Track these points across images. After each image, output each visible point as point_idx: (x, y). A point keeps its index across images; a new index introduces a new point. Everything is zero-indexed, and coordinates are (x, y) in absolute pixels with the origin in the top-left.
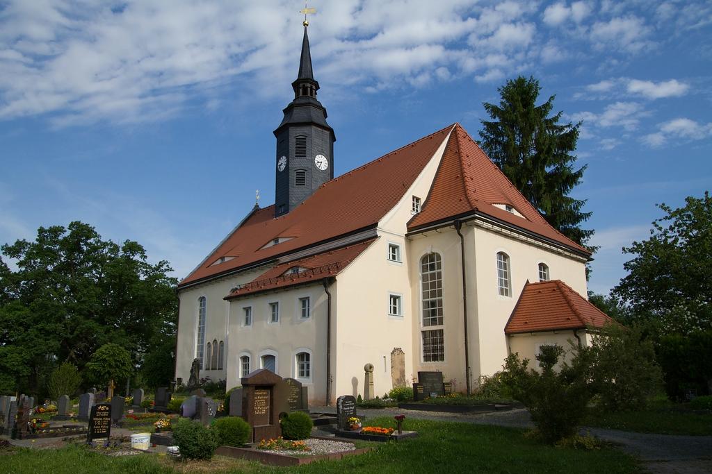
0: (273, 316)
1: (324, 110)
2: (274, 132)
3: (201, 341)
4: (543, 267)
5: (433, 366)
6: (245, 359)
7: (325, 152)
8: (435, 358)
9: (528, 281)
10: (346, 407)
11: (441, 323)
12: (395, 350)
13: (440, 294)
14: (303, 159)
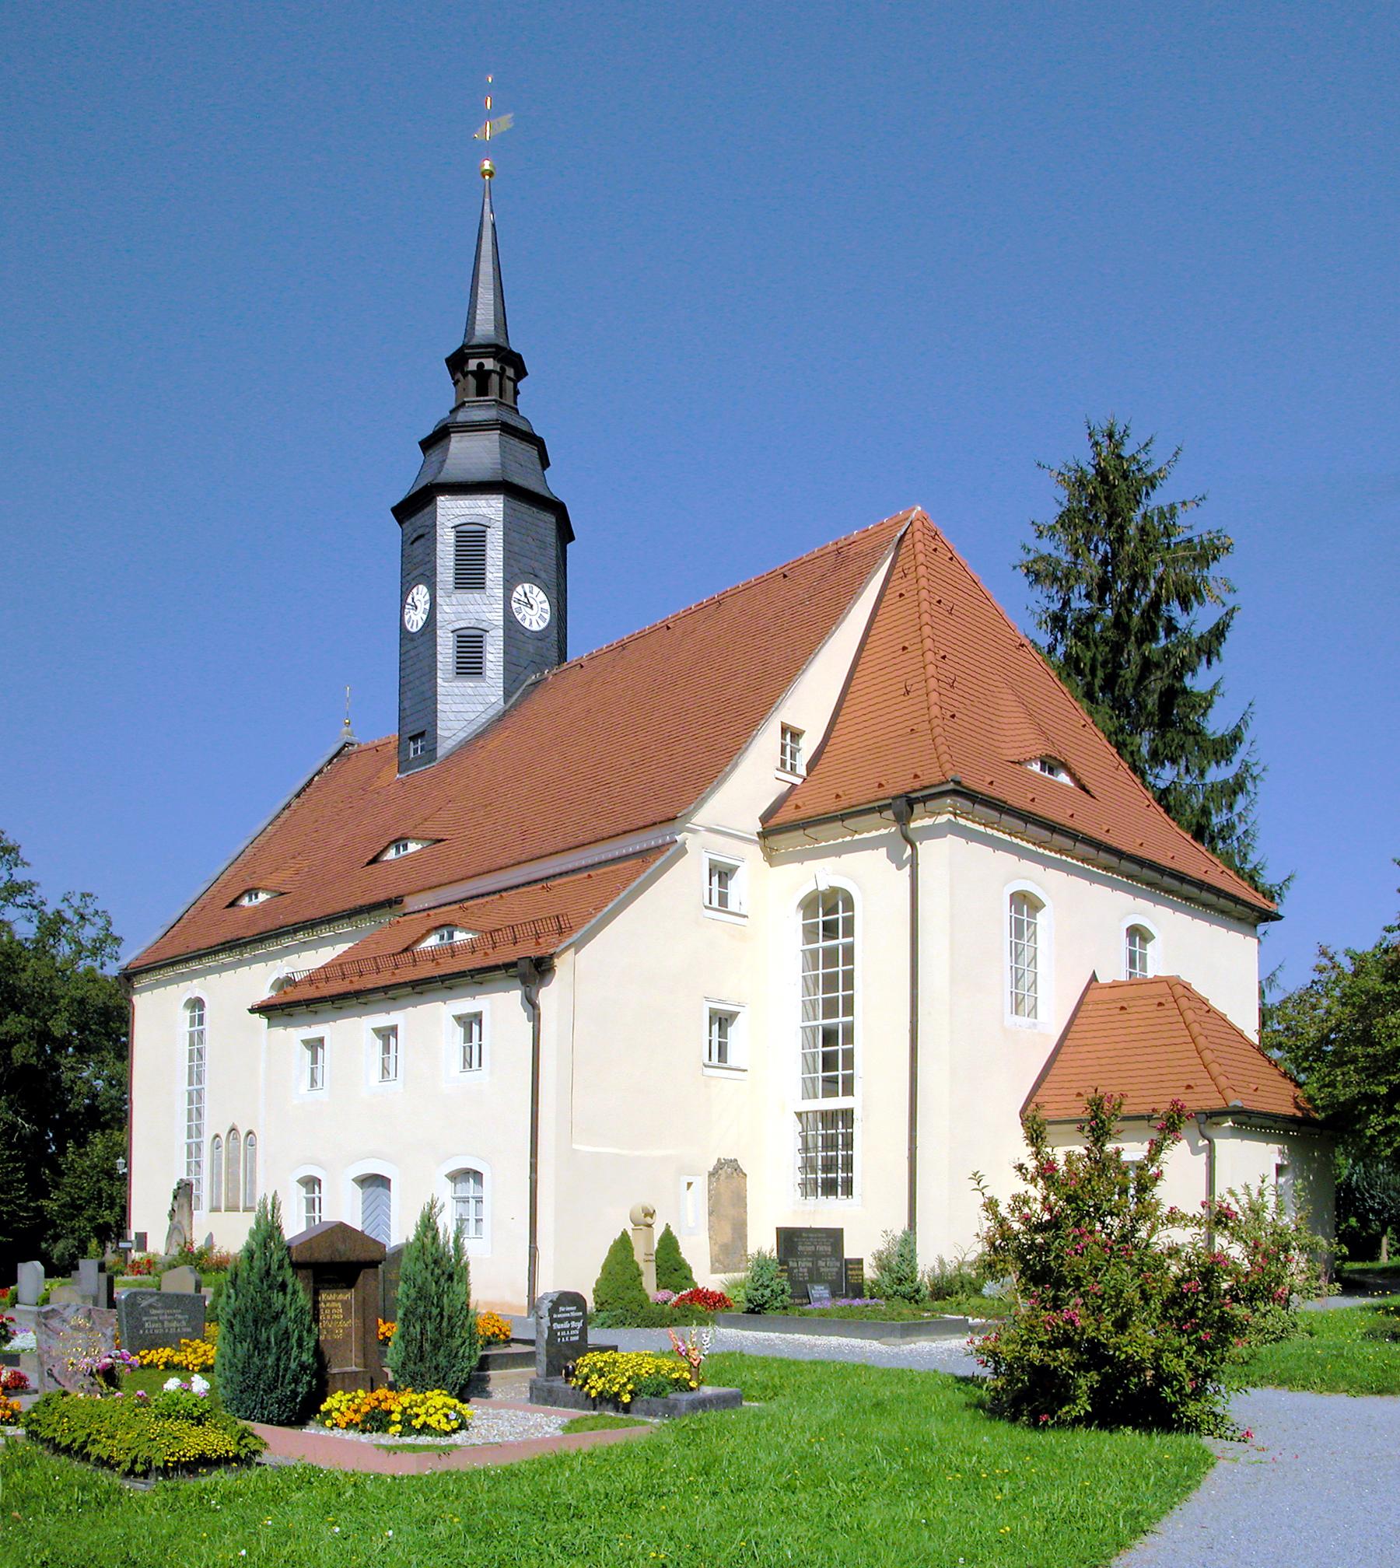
0: (385, 1069)
1: (538, 443)
2: (448, 360)
3: (194, 1131)
4: (1138, 934)
5: (823, 1213)
6: (311, 1183)
7: (543, 575)
8: (830, 1188)
9: (1094, 978)
10: (560, 1321)
11: (849, 1090)
12: (721, 1165)
13: (849, 1009)
14: (475, 596)
